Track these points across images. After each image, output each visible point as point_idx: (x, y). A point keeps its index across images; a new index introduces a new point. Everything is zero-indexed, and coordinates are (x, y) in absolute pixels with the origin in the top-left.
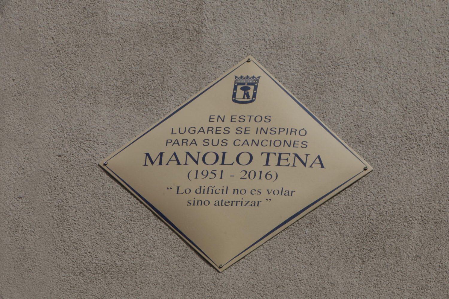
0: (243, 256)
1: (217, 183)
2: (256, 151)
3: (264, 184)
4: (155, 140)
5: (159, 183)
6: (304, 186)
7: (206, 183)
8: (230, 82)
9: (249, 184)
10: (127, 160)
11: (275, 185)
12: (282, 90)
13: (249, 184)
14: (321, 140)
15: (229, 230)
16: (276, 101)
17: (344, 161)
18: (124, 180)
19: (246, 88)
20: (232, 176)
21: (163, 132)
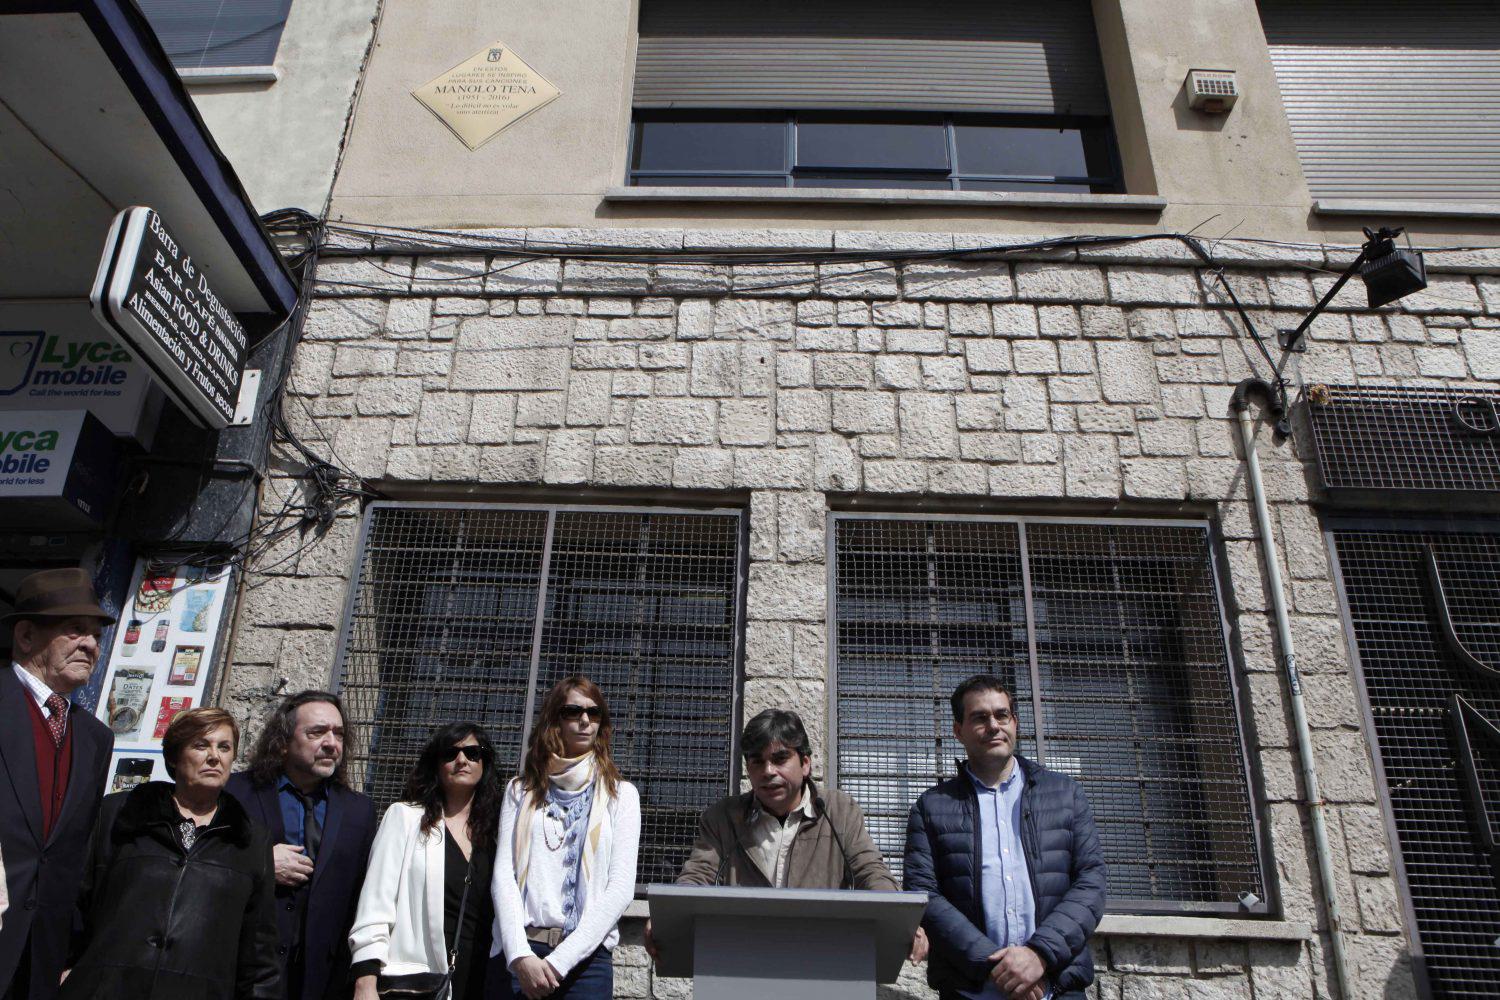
0: (487, 141)
1: (475, 102)
2: (498, 85)
3: (501, 102)
4: (442, 82)
5: (441, 103)
6: (523, 102)
7: (469, 102)
8: (487, 51)
9: (492, 102)
10: (426, 90)
11: (508, 102)
12: (764, 127)
13: (492, 102)
14: (533, 79)
15: (477, 126)
16: (511, 61)
17: (547, 89)
18: (204, 145)
19: (496, 54)
20: (484, 98)
21: (448, 76)
